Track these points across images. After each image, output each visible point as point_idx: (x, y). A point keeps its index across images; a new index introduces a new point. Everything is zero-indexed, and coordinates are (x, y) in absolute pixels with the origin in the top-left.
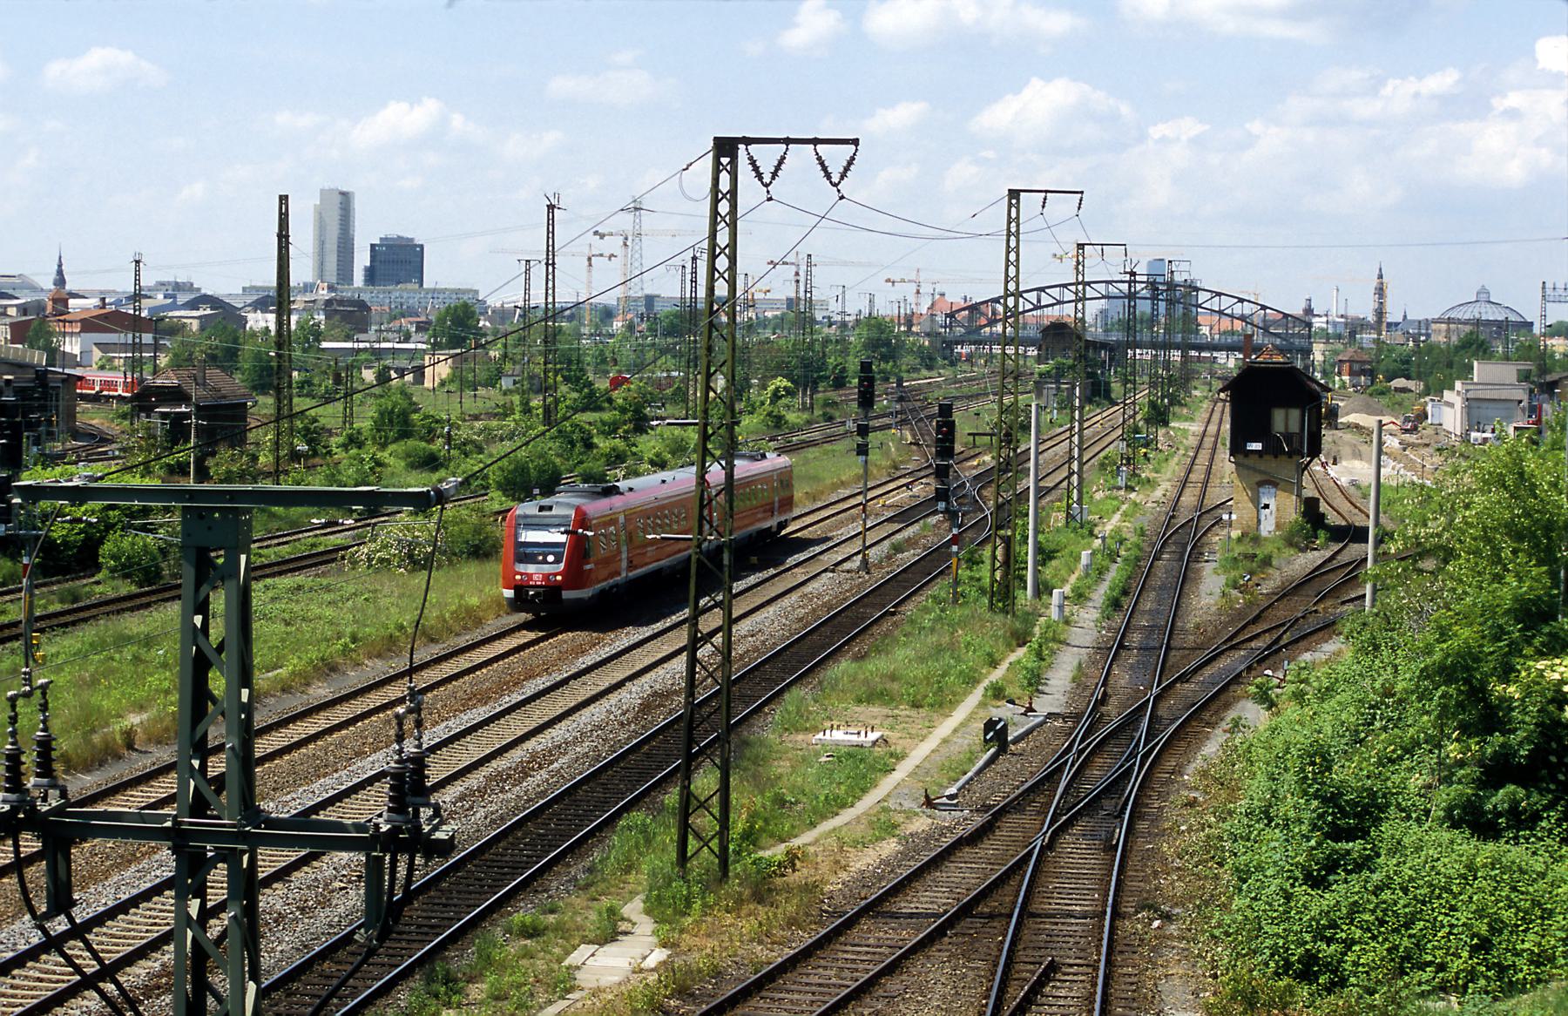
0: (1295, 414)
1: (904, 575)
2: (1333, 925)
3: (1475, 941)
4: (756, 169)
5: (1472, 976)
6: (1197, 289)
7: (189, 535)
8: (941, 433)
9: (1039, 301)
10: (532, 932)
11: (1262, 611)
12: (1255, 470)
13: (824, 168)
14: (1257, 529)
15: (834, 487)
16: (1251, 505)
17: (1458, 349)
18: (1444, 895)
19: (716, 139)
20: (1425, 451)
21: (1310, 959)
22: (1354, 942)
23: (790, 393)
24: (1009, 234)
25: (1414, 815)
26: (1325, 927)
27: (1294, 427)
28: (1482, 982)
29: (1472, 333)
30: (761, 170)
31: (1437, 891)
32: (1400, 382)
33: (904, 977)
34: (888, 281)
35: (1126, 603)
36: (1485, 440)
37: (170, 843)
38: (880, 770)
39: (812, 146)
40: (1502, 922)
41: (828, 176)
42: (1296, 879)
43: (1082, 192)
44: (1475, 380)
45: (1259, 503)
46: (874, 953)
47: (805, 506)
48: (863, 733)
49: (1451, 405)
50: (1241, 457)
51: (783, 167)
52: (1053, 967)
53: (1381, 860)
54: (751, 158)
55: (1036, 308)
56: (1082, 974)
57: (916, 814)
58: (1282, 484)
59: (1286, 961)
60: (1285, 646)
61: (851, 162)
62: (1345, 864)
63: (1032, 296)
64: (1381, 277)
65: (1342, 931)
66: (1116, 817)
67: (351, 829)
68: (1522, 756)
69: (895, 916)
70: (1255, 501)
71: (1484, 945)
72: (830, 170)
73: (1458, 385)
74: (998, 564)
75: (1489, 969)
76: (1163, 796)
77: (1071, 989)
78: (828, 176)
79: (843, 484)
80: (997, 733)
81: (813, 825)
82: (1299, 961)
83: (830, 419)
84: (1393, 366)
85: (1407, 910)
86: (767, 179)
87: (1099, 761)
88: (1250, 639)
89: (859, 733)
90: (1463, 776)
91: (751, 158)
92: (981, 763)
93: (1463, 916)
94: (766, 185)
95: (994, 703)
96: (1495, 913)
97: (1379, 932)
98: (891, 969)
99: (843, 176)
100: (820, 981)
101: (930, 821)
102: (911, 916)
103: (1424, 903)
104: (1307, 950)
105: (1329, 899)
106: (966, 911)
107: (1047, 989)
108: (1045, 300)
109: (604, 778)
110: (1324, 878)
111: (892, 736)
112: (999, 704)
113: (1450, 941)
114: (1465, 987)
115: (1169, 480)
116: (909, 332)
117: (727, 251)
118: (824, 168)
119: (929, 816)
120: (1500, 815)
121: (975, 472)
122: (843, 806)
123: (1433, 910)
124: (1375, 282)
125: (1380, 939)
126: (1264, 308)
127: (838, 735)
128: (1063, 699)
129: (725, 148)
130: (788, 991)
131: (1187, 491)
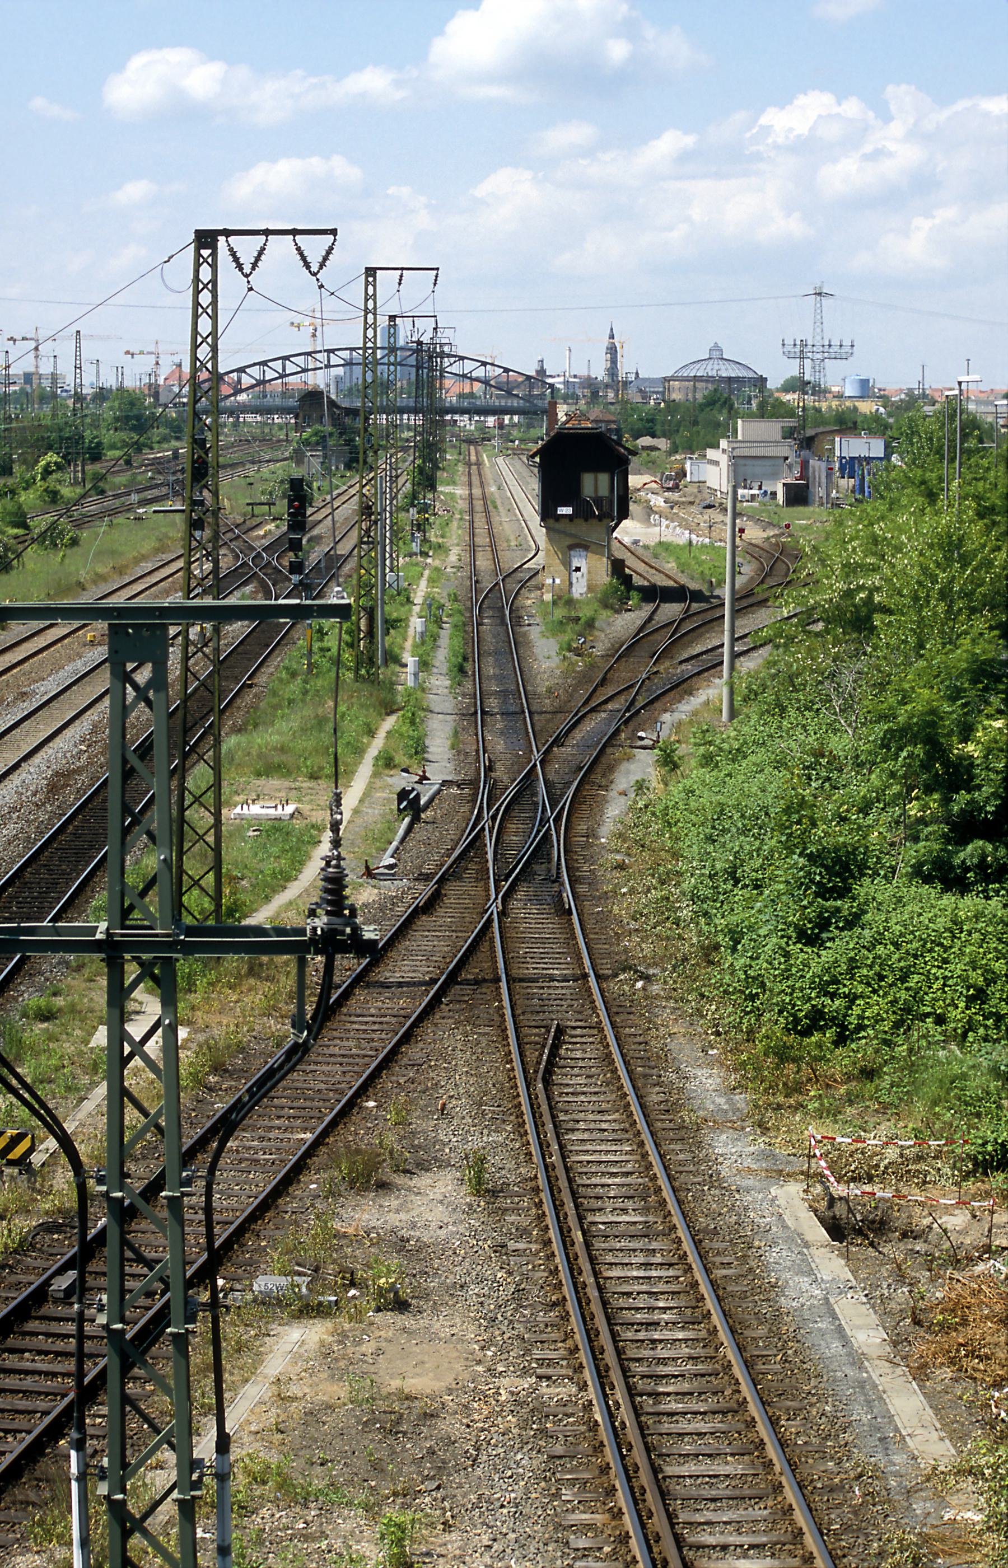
0: (604, 478)
1: (242, 647)
2: (835, 981)
3: (972, 991)
4: (236, 260)
5: (970, 1026)
6: (442, 355)
7: (116, 652)
8: (293, 507)
9: (284, 370)
10: (46, 1016)
11: (606, 673)
12: (564, 533)
13: (303, 258)
14: (570, 591)
15: (138, 560)
16: (562, 568)
17: (702, 407)
18: (936, 949)
19: (197, 232)
20: (693, 509)
21: (817, 1015)
22: (856, 997)
23: (59, 467)
24: (366, 311)
25: (882, 873)
26: (829, 983)
27: (604, 491)
28: (981, 1031)
29: (716, 390)
30: (241, 261)
31: (929, 945)
32: (646, 441)
33: (421, 1045)
34: (127, 353)
35: (468, 667)
36: (753, 496)
37: (103, 955)
38: (309, 842)
39: (291, 237)
40: (994, 973)
41: (307, 265)
42: (790, 938)
43: (438, 269)
44: (740, 438)
45: (570, 566)
46: (381, 1023)
47: (114, 581)
48: (280, 807)
49: (716, 463)
50: (551, 522)
51: (263, 257)
52: (560, 1031)
53: (868, 916)
54: (231, 250)
55: (282, 376)
56: (590, 1036)
57: (361, 885)
58: (593, 547)
59: (794, 1015)
60: (643, 708)
61: (329, 251)
62: (836, 922)
63: (278, 365)
64: (612, 337)
65: (845, 986)
66: (554, 882)
67: (272, 932)
68: (989, 812)
69: (386, 986)
70: (567, 563)
71: (980, 996)
72: (309, 259)
73: (724, 443)
74: (362, 635)
75: (986, 1018)
76: (591, 860)
77: (584, 1051)
78: (307, 265)
79: (144, 558)
80: (410, 802)
81: (267, 899)
82: (806, 1017)
83: (102, 492)
84: (639, 425)
85: (902, 964)
86: (247, 269)
87: (512, 827)
88: (606, 702)
89: (276, 807)
90: (930, 833)
91: (231, 250)
92: (401, 832)
93: (958, 968)
94: (247, 276)
95: (387, 772)
96: (986, 965)
97: (880, 987)
98: (407, 1038)
99: (322, 265)
100: (342, 1052)
101: (376, 891)
102: (400, 985)
103: (915, 956)
104: (813, 1006)
105: (826, 956)
106: (452, 978)
107: (562, 1052)
108: (290, 368)
109: (43, 859)
110: (818, 935)
111: (305, 808)
112: (392, 773)
113: (945, 992)
114: (965, 1035)
115: (458, 545)
116: (157, 403)
117: (209, 340)
118: (303, 258)
119: (374, 887)
120: (968, 869)
121: (266, 542)
122: (288, 879)
123: (925, 963)
124: (606, 342)
125: (881, 993)
126: (507, 370)
127: (256, 809)
128: (451, 766)
129: (206, 239)
130: (316, 1063)
131: (480, 555)
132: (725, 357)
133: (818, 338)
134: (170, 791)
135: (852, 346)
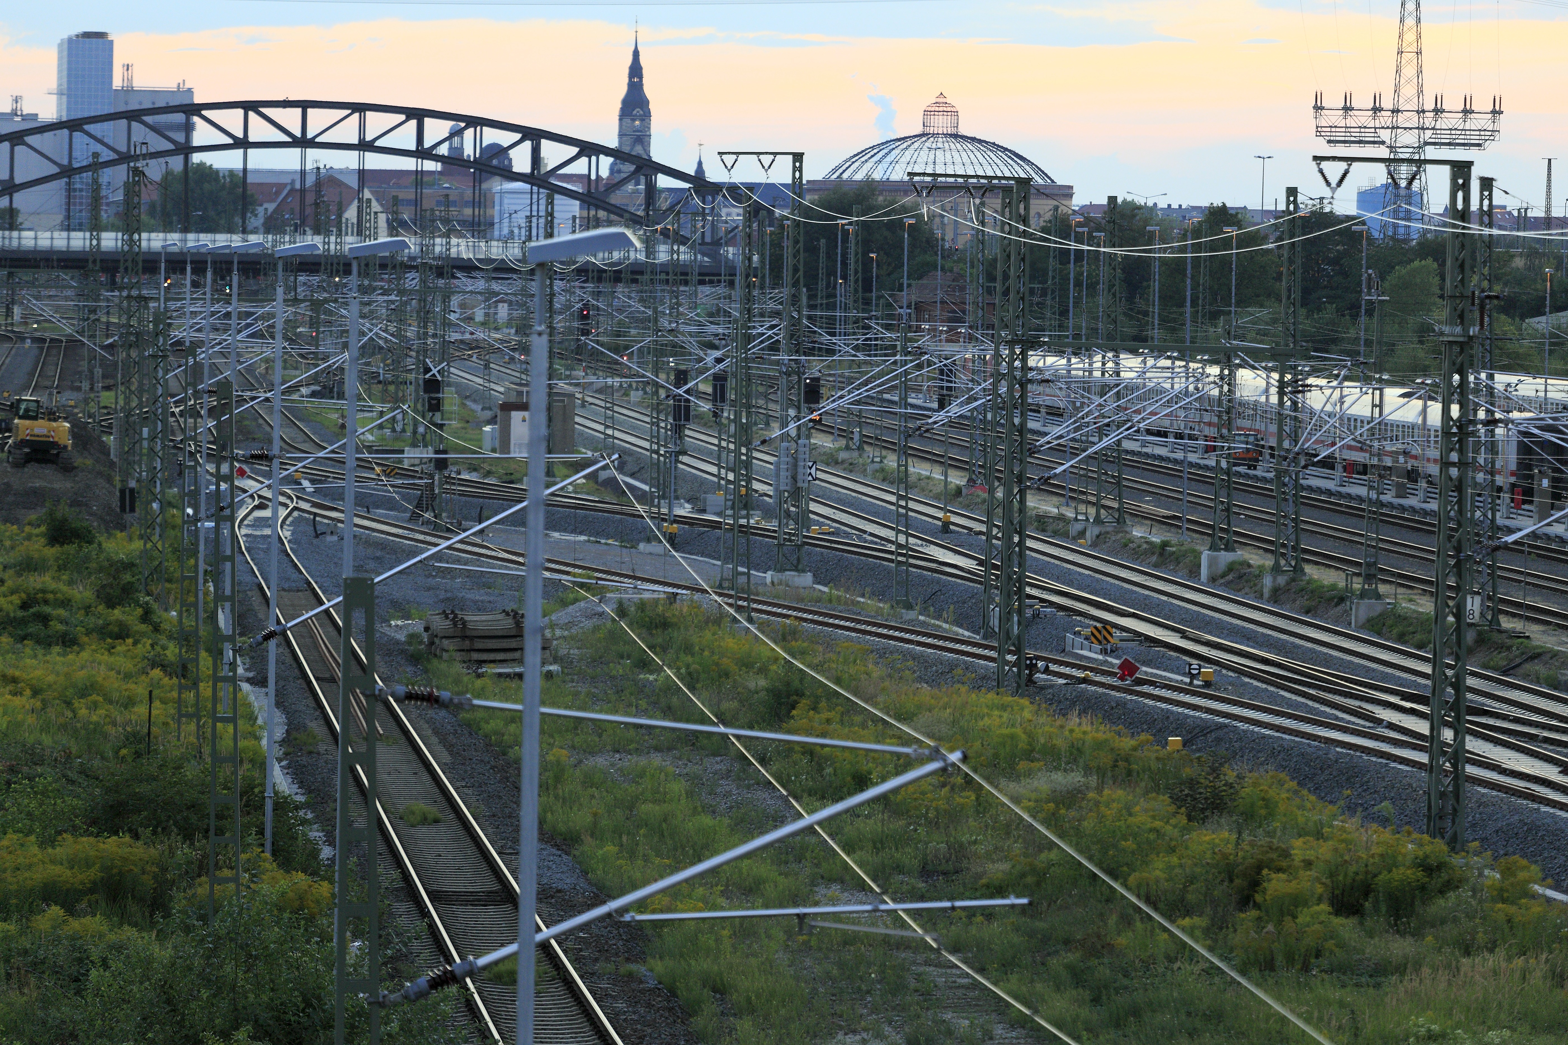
124: (633, 48)
132: (963, 131)
133: (1408, 91)
134: (606, 544)
135: (1496, 113)
